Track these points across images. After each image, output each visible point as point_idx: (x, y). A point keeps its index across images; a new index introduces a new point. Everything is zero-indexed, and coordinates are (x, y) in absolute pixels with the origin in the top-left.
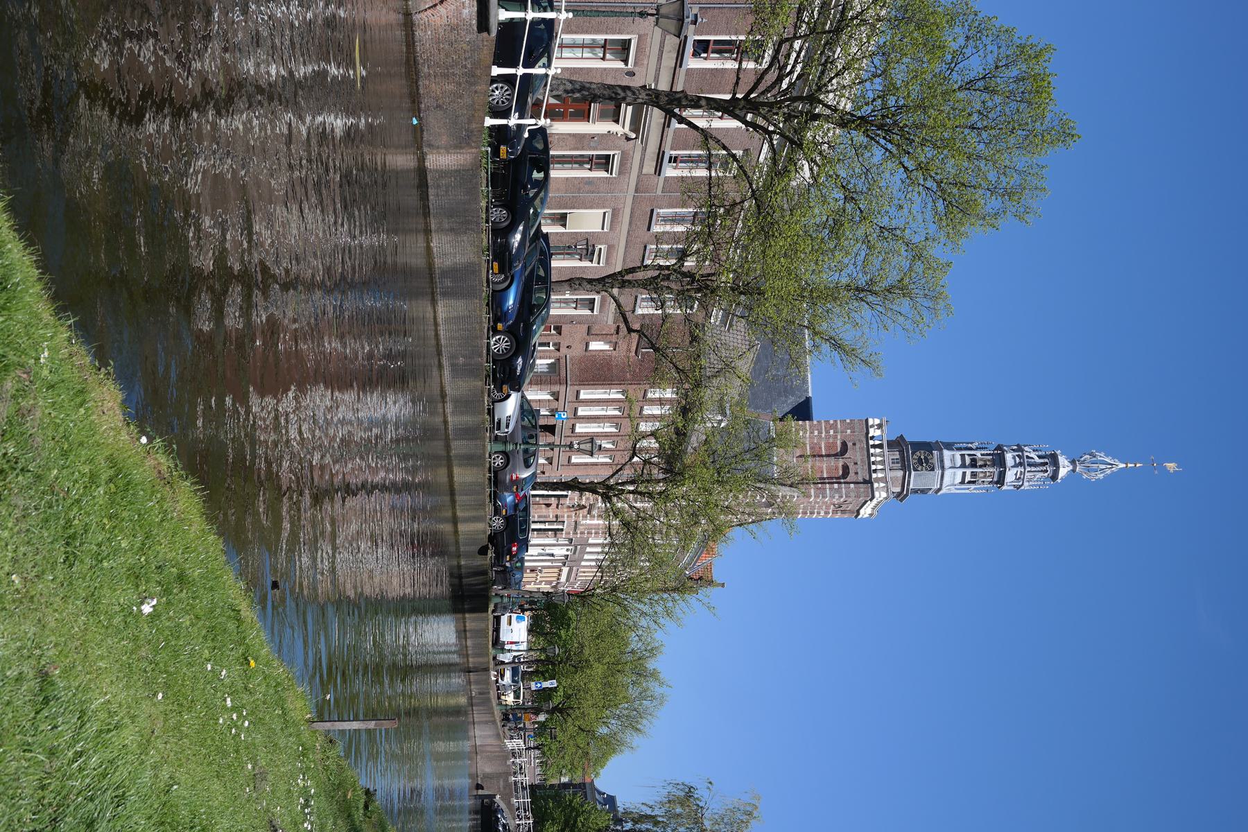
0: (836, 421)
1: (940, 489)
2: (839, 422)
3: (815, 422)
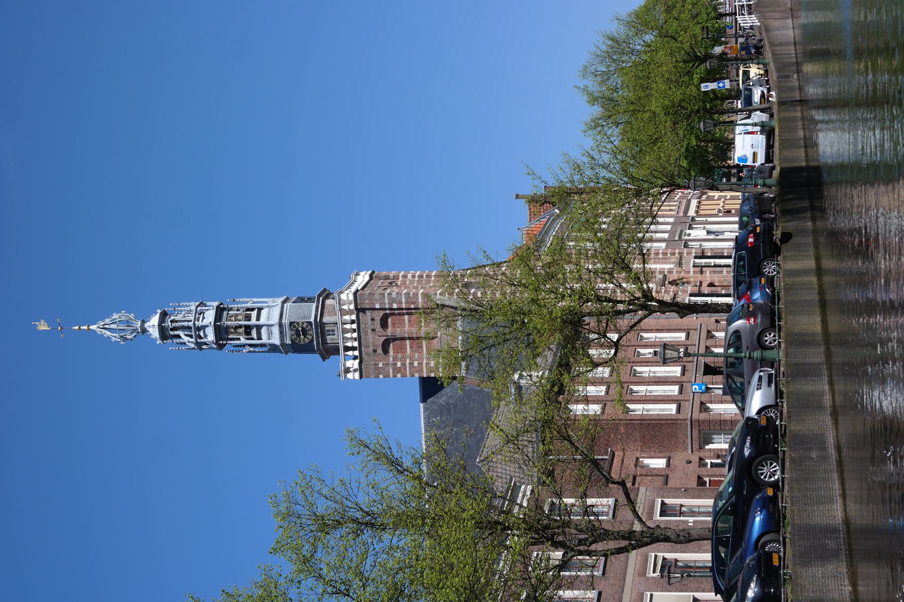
0: (395, 376)
1: (284, 302)
2: (391, 375)
3: (417, 375)
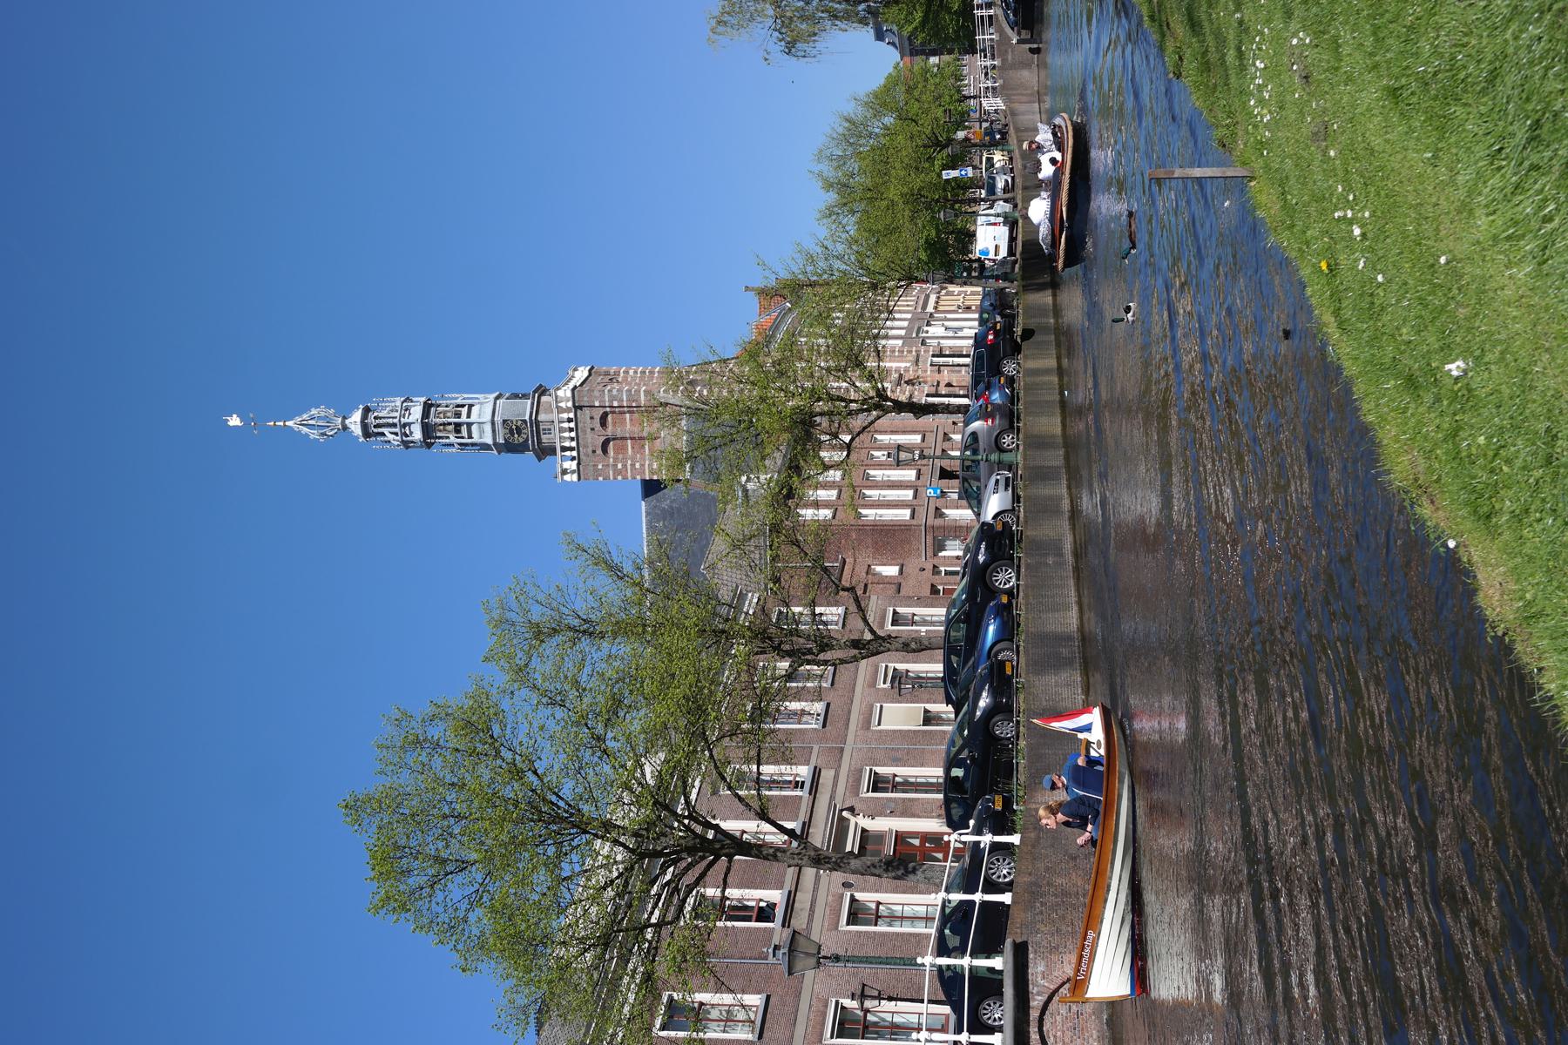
0: (615, 478)
